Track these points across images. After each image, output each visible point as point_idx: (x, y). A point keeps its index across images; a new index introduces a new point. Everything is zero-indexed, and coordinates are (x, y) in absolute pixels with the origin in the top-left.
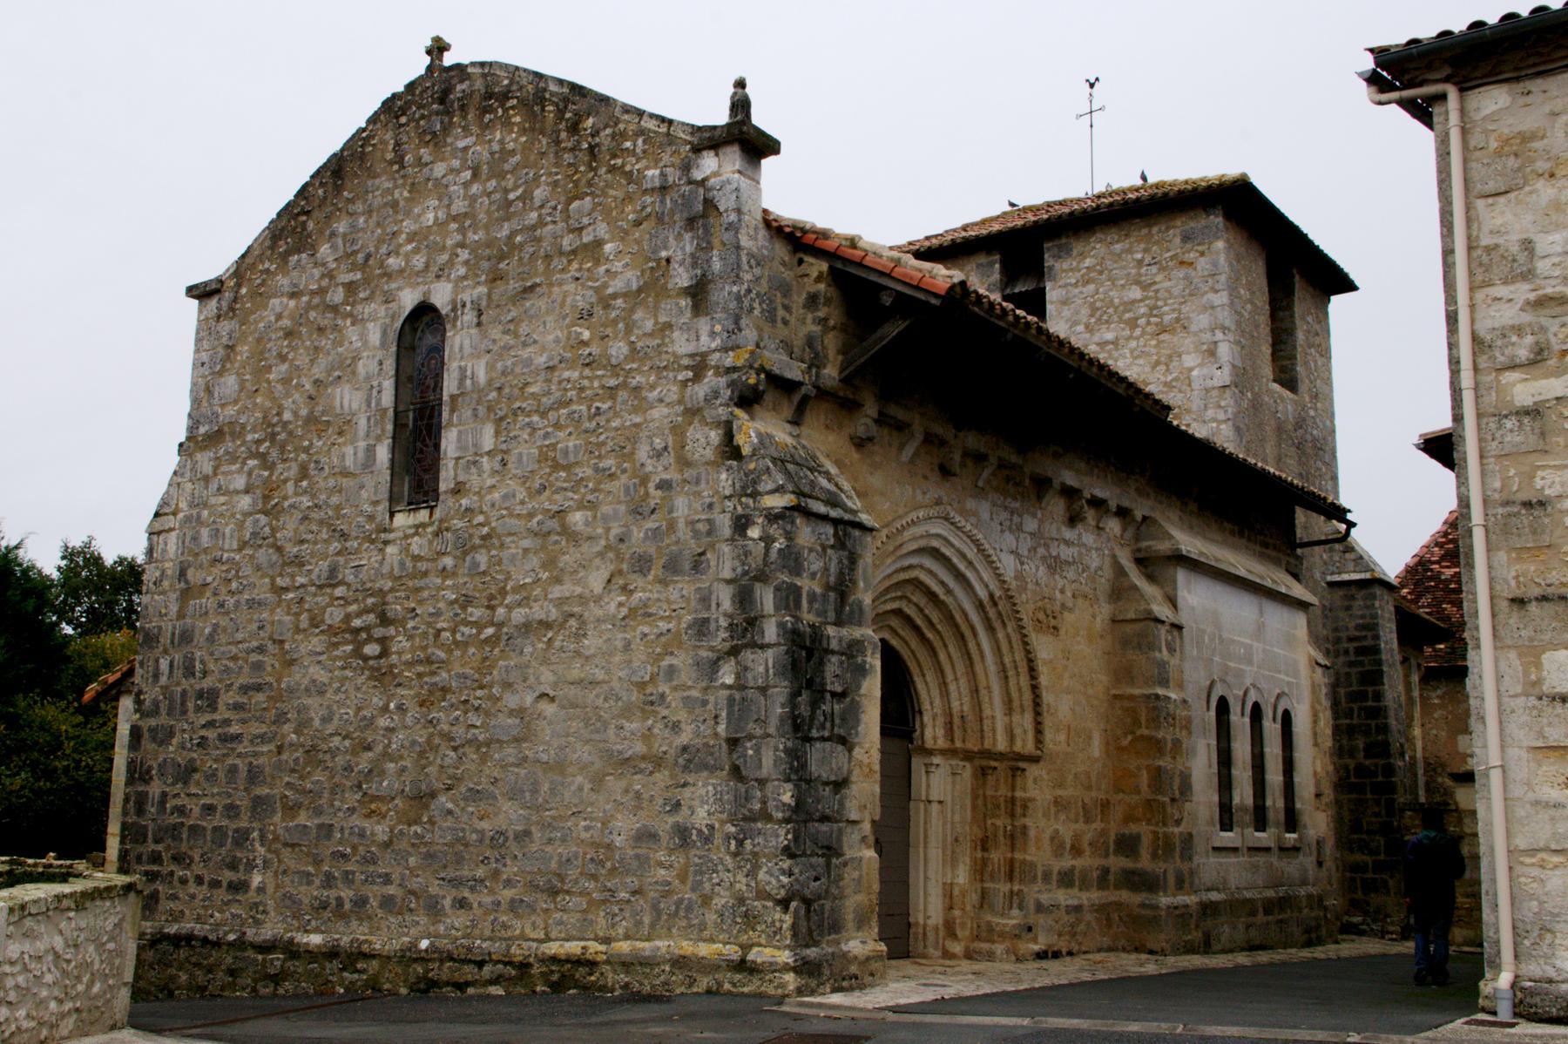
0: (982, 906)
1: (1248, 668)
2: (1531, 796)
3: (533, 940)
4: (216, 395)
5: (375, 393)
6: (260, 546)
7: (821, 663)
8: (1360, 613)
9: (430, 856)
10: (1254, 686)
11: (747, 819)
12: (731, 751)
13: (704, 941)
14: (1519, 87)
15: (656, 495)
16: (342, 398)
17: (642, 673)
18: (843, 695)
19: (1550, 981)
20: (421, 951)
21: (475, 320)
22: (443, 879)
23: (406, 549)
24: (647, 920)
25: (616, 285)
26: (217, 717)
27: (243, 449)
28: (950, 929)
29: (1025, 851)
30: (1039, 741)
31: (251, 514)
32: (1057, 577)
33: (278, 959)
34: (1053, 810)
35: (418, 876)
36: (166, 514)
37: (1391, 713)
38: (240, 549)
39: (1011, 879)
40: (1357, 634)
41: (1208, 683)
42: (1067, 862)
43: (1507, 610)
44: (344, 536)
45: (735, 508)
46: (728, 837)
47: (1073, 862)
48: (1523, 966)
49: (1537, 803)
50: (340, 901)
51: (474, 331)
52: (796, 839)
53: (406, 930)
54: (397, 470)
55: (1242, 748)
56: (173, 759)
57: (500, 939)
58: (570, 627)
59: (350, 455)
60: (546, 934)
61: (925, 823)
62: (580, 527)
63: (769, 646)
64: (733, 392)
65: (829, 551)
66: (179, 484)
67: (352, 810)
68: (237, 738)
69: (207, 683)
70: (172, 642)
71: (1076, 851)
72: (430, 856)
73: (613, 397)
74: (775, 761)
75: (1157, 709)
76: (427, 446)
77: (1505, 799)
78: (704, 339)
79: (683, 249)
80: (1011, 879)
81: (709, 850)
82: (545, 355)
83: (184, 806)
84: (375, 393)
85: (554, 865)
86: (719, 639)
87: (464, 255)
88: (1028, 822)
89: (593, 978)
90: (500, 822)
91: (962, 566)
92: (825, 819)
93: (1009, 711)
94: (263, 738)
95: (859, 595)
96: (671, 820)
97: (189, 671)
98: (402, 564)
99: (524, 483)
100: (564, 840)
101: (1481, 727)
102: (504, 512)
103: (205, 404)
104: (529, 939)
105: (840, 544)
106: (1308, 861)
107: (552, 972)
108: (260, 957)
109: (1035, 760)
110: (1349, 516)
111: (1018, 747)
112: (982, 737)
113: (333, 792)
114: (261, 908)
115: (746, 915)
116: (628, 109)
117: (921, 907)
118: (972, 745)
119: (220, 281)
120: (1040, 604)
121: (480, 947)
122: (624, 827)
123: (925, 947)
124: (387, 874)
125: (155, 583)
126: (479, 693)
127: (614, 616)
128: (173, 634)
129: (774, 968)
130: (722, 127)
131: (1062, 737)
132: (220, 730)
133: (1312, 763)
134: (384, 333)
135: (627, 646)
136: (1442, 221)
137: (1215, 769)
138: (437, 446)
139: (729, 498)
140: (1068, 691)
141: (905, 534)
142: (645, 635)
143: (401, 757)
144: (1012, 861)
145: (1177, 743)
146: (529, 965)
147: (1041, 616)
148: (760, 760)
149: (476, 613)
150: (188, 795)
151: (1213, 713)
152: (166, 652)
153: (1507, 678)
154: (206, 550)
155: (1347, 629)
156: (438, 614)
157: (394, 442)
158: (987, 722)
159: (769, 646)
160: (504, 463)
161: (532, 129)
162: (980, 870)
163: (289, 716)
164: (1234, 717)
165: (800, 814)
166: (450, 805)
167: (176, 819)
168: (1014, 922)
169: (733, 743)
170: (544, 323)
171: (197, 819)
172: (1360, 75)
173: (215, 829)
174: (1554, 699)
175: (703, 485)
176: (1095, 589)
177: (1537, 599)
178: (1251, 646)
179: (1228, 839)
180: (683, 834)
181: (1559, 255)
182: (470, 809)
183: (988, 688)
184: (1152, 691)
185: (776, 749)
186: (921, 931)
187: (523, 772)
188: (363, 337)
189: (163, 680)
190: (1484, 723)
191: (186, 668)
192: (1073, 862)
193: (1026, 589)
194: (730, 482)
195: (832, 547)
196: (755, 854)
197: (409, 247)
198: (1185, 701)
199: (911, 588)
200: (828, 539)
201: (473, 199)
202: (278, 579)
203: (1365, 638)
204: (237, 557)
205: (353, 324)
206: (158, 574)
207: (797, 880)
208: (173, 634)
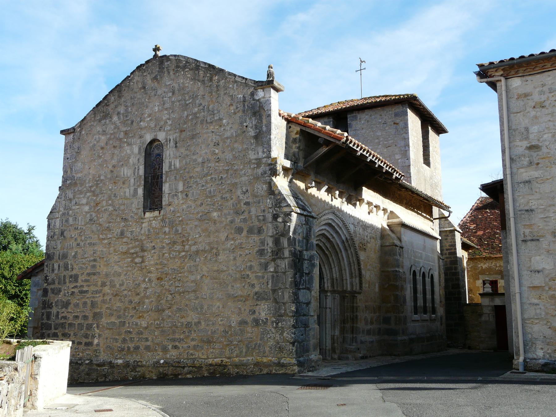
0: (343, 342)
1: (421, 261)
2: (528, 302)
3: (203, 359)
4: (73, 170)
5: (136, 170)
6: (93, 224)
7: (302, 264)
8: (450, 241)
9: (163, 331)
10: (423, 266)
11: (279, 317)
12: (273, 294)
13: (265, 357)
14: (524, 78)
15: (244, 207)
16: (124, 172)
17: (240, 268)
18: (309, 274)
19: (535, 359)
20: (161, 364)
21: (174, 146)
22: (168, 339)
23: (150, 225)
24: (244, 351)
25: (228, 134)
26: (78, 284)
27: (85, 189)
28: (333, 350)
29: (357, 324)
30: (361, 287)
31: (89, 212)
32: (365, 232)
33: (106, 369)
34: (365, 309)
35: (159, 338)
36: (54, 212)
37: (460, 274)
38: (85, 225)
39: (353, 333)
40: (449, 248)
41: (410, 266)
42: (369, 327)
43: (521, 244)
44: (125, 220)
45: (273, 212)
46: (273, 322)
47: (371, 327)
48: (526, 355)
49: (531, 304)
50: (129, 348)
51: (174, 149)
52: (296, 322)
53: (155, 357)
54: (145, 197)
55: (420, 287)
56: (61, 300)
57: (191, 359)
58: (213, 252)
59: (128, 192)
60: (207, 357)
61: (325, 315)
62: (216, 218)
63: (286, 258)
64: (271, 172)
65: (304, 226)
66: (59, 201)
67: (132, 316)
68: (86, 292)
69: (74, 272)
70: (59, 258)
71: (372, 323)
72: (163, 331)
73: (227, 173)
74: (289, 297)
75: (396, 276)
76: (156, 189)
77: (521, 303)
78: (260, 153)
79: (252, 123)
80: (353, 333)
81: (266, 326)
82: (201, 158)
83: (66, 316)
84: (136, 170)
85: (209, 333)
86: (268, 256)
87: (170, 122)
88: (358, 314)
89: (225, 371)
90: (189, 319)
91: (338, 229)
92: (304, 315)
93: (351, 277)
94: (97, 292)
95: (312, 240)
96: (252, 317)
97: (66, 268)
98: (149, 230)
99: (195, 202)
100: (213, 324)
101: (513, 281)
102: (187, 212)
103: (69, 172)
104: (201, 359)
105: (307, 223)
106: (438, 323)
107: (210, 369)
108: (99, 368)
109: (359, 293)
110: (450, 209)
111: (354, 289)
112: (343, 286)
113: (125, 311)
114: (98, 351)
115: (280, 348)
116: (230, 74)
117: (324, 343)
118: (340, 289)
119: (73, 128)
120: (360, 241)
121: (183, 362)
122: (235, 320)
123: (326, 356)
124: (146, 338)
125: (51, 237)
126: (180, 275)
127: (229, 249)
128: (59, 255)
129: (290, 365)
130: (265, 81)
131: (367, 285)
132: (79, 289)
133: (439, 291)
134: (140, 149)
135: (235, 259)
136: (500, 121)
137: (412, 295)
138: (161, 189)
139: (271, 208)
140: (369, 270)
141: (322, 219)
142: (241, 255)
143: (151, 298)
144: (353, 327)
145: (402, 286)
146: (202, 367)
147: (361, 245)
148: (284, 296)
149: (178, 247)
150: (68, 312)
151: (412, 276)
152: (57, 262)
153: (521, 265)
154: (71, 225)
155: (446, 246)
156: (163, 247)
157: (144, 187)
158: (345, 281)
159: (286, 258)
160: (187, 195)
161: (194, 79)
162: (343, 330)
163: (107, 284)
164: (427, 279)
165: (297, 313)
166: (170, 314)
167: (63, 321)
168: (353, 347)
169: (274, 291)
170: (201, 147)
171: (71, 320)
172: (475, 73)
173: (79, 324)
174: (535, 272)
175: (261, 204)
176: (376, 236)
177: (530, 240)
178: (422, 253)
179: (416, 317)
180: (256, 322)
181: (536, 133)
182: (178, 315)
183: (345, 270)
184: (395, 269)
185: (289, 293)
186: (324, 351)
187: (197, 302)
188: (132, 150)
189: (56, 272)
190: (514, 280)
191: (65, 268)
192: (371, 327)
193: (356, 236)
194: (271, 203)
195: (304, 224)
196: (282, 328)
197: (149, 119)
198: (404, 272)
199: (321, 236)
200: (303, 222)
201: (173, 102)
202: (101, 236)
203: (452, 249)
204: (84, 228)
205: (127, 146)
206: (52, 234)
207: (297, 336)
208: (59, 255)
